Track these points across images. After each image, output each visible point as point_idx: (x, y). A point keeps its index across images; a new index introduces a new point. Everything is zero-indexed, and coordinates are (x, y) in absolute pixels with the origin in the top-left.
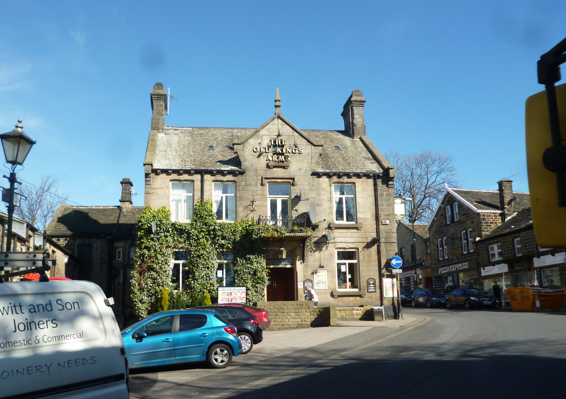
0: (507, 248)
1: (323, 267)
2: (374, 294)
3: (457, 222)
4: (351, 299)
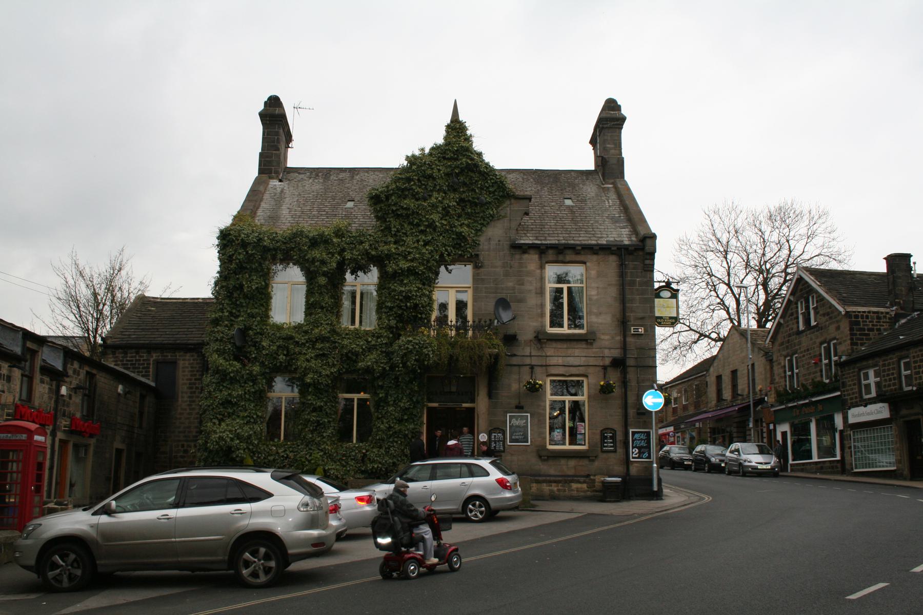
0: (888, 375)
3: (815, 326)
4: (572, 463)
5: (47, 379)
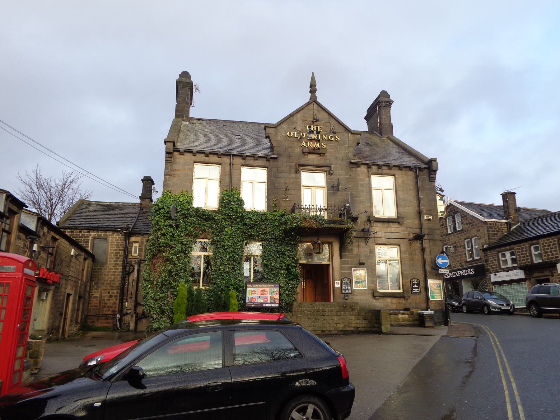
1: (363, 264)
2: (418, 297)
3: (459, 231)
5: (23, 236)
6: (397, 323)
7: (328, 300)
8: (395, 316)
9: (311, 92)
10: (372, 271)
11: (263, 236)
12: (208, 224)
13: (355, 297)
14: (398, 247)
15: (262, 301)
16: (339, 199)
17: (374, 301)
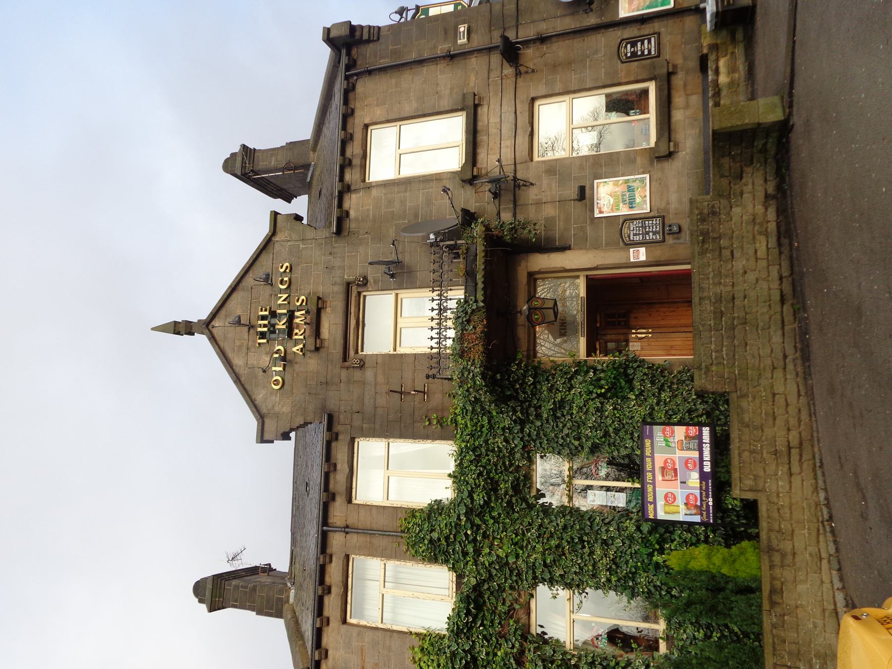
1: (582, 189)
2: (666, 39)
6: (742, 88)
7: (686, 277)
8: (724, 93)
9: (191, 333)
10: (603, 164)
11: (518, 456)
12: (489, 601)
13: (673, 206)
14: (537, 103)
15: (695, 476)
16: (419, 259)
17: (681, 154)
